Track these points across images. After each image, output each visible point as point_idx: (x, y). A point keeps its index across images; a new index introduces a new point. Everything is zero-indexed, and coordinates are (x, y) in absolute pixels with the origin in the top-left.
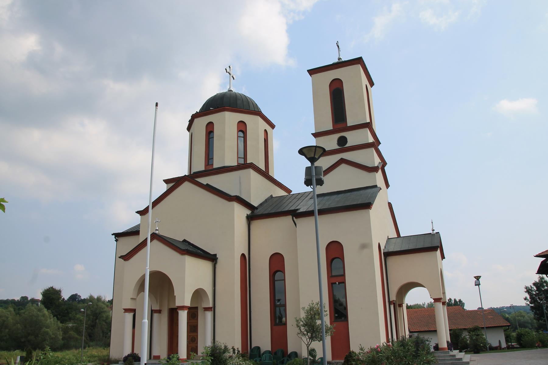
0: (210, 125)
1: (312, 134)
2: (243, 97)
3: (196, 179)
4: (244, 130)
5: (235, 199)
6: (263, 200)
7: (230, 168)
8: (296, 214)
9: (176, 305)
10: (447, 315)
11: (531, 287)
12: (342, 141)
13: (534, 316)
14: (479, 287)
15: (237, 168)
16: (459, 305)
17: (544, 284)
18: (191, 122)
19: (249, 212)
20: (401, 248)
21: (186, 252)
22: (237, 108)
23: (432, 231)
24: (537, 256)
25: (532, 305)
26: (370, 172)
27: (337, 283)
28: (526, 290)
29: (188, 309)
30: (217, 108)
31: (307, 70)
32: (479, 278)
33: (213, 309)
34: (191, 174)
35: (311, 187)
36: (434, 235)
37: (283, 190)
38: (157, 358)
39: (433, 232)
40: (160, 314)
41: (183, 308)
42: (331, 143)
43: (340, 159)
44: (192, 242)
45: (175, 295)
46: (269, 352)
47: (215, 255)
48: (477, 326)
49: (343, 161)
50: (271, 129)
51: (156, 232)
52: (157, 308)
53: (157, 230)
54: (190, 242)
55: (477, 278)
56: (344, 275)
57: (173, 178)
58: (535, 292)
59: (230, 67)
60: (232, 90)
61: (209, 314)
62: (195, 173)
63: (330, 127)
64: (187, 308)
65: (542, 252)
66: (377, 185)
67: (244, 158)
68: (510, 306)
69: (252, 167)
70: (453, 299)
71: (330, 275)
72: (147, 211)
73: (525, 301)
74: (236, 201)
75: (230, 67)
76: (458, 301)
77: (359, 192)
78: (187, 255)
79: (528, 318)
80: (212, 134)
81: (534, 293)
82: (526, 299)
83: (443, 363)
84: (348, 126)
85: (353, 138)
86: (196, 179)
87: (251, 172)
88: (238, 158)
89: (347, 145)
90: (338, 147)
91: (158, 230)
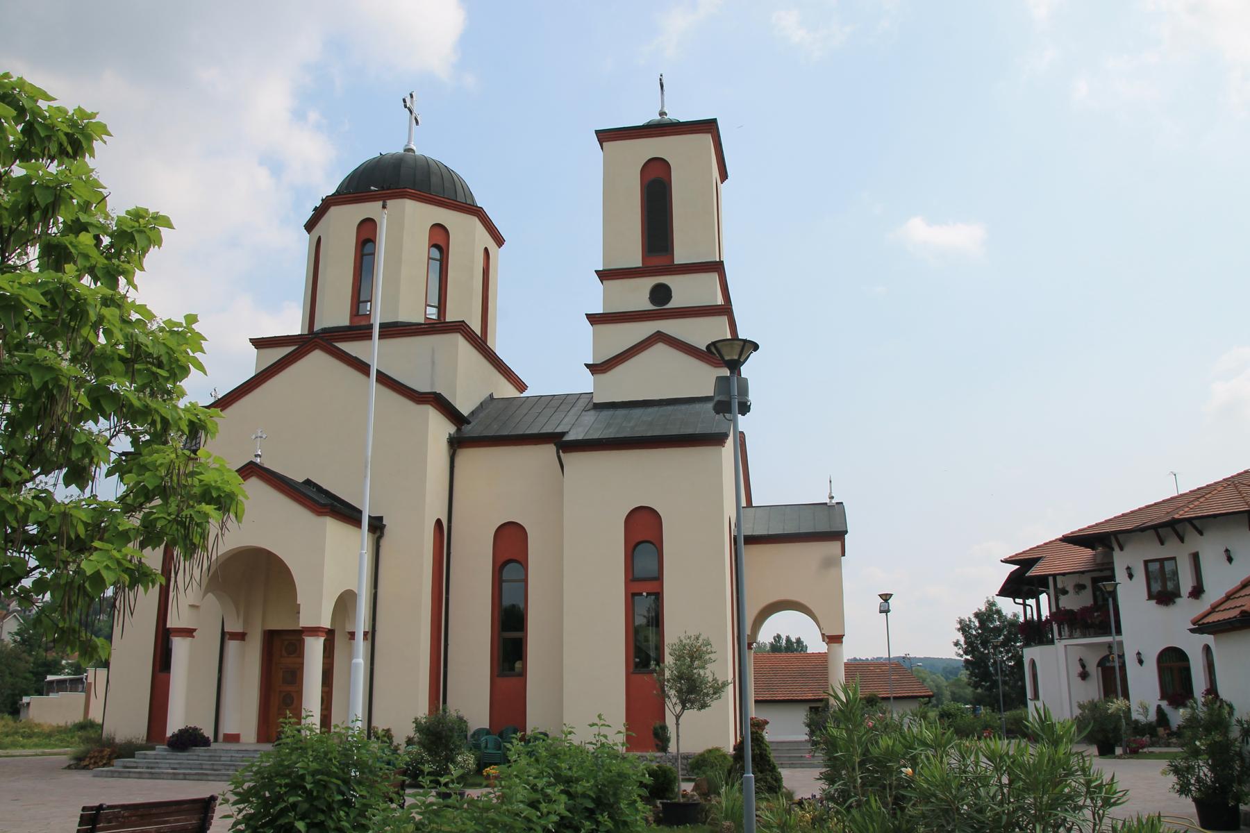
0: (366, 235)
2: (442, 170)
4: (441, 244)
5: (431, 399)
8: (564, 444)
9: (301, 625)
11: (970, 621)
12: (661, 294)
13: (970, 679)
14: (887, 615)
16: (796, 650)
17: (995, 616)
20: (768, 530)
22: (430, 194)
23: (830, 498)
24: (1006, 561)
25: (969, 657)
26: (716, 367)
27: (645, 594)
28: (959, 626)
29: (324, 634)
30: (388, 189)
31: (596, 131)
32: (888, 598)
34: (316, 329)
35: (724, 416)
37: (511, 383)
38: (234, 738)
41: (314, 631)
42: (637, 295)
43: (655, 333)
44: (325, 487)
45: (298, 603)
46: (488, 732)
48: (875, 695)
50: (496, 245)
52: (234, 626)
53: (259, 455)
54: (321, 485)
55: (884, 598)
56: (659, 578)
57: (288, 336)
58: (975, 631)
59: (411, 96)
60: (414, 148)
62: (325, 331)
63: (636, 261)
64: (322, 631)
65: (1017, 555)
68: (904, 658)
69: (463, 331)
70: (784, 637)
71: (631, 578)
73: (956, 649)
75: (411, 96)
76: (794, 640)
77: (691, 406)
78: (331, 516)
79: (931, 683)
80: (369, 245)
81: (974, 633)
82: (957, 644)
85: (685, 290)
87: (460, 340)
88: (427, 305)
89: (669, 306)
91: (260, 456)
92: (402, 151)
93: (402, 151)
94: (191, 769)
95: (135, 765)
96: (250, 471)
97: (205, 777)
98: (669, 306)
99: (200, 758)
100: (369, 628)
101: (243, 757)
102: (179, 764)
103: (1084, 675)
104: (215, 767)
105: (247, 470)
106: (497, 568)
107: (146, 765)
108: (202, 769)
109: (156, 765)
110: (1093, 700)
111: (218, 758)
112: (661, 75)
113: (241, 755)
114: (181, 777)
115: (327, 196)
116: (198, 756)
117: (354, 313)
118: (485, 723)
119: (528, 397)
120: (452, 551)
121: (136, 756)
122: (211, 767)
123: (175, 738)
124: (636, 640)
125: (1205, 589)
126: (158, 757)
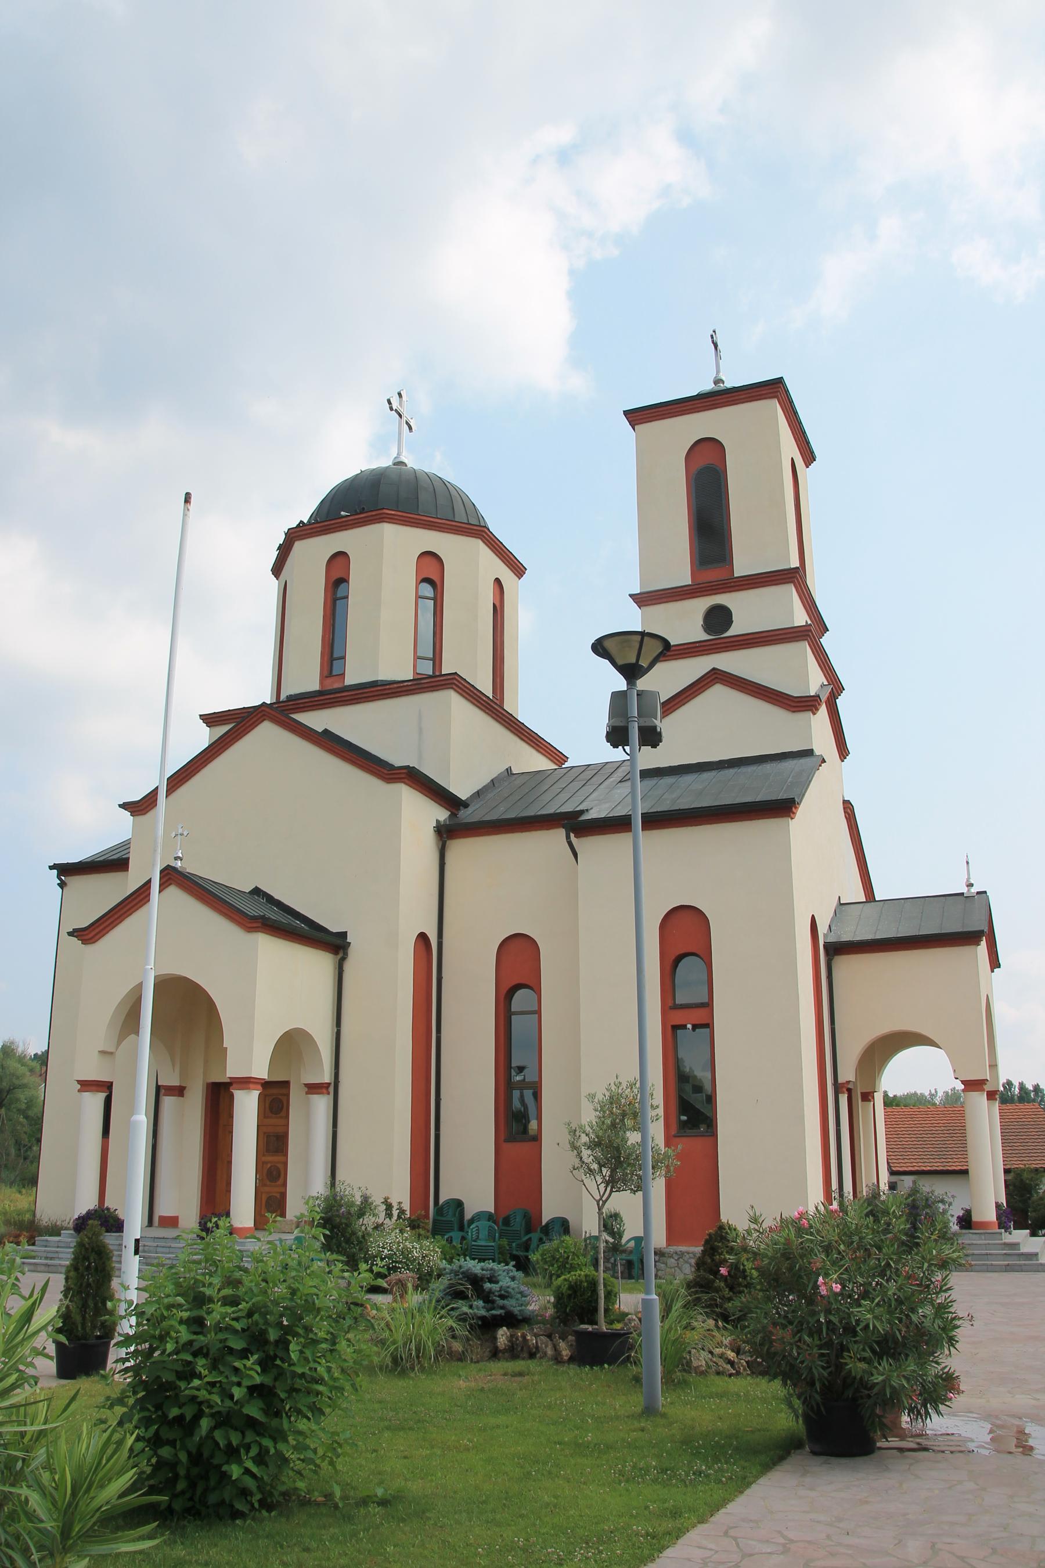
0: (340, 559)
1: (630, 596)
3: (295, 716)
4: (435, 578)
6: (486, 780)
7: (392, 686)
9: (228, 1076)
10: (999, 1128)
15: (413, 687)
16: (1034, 1101)
18: (285, 550)
19: (442, 814)
21: (259, 925)
23: (967, 886)
26: (794, 712)
27: (689, 1026)
29: (260, 1087)
35: (624, 750)
39: (968, 890)
40: (180, 1098)
41: (245, 1083)
44: (276, 897)
46: (490, 1217)
47: (344, 935)
49: (716, 678)
51: (176, 864)
52: (171, 1080)
53: (179, 857)
56: (708, 1005)
59: (400, 395)
60: (406, 461)
61: (321, 1104)
62: (291, 698)
63: (684, 578)
67: (434, 660)
74: (406, 780)
75: (400, 395)
77: (760, 767)
80: (343, 586)
83: (984, 1265)
84: (735, 575)
86: (295, 716)
87: (453, 699)
88: (416, 658)
90: (705, 637)
96: (167, 878)
100: (331, 1079)
101: (157, 1246)
103: (125, 1247)
106: (502, 997)
107: (45, 1255)
113: (155, 1244)
115: (289, 529)
117: (326, 673)
120: (444, 975)
121: (37, 1243)
123: (81, 1221)
124: (680, 1090)
125: (254, 887)
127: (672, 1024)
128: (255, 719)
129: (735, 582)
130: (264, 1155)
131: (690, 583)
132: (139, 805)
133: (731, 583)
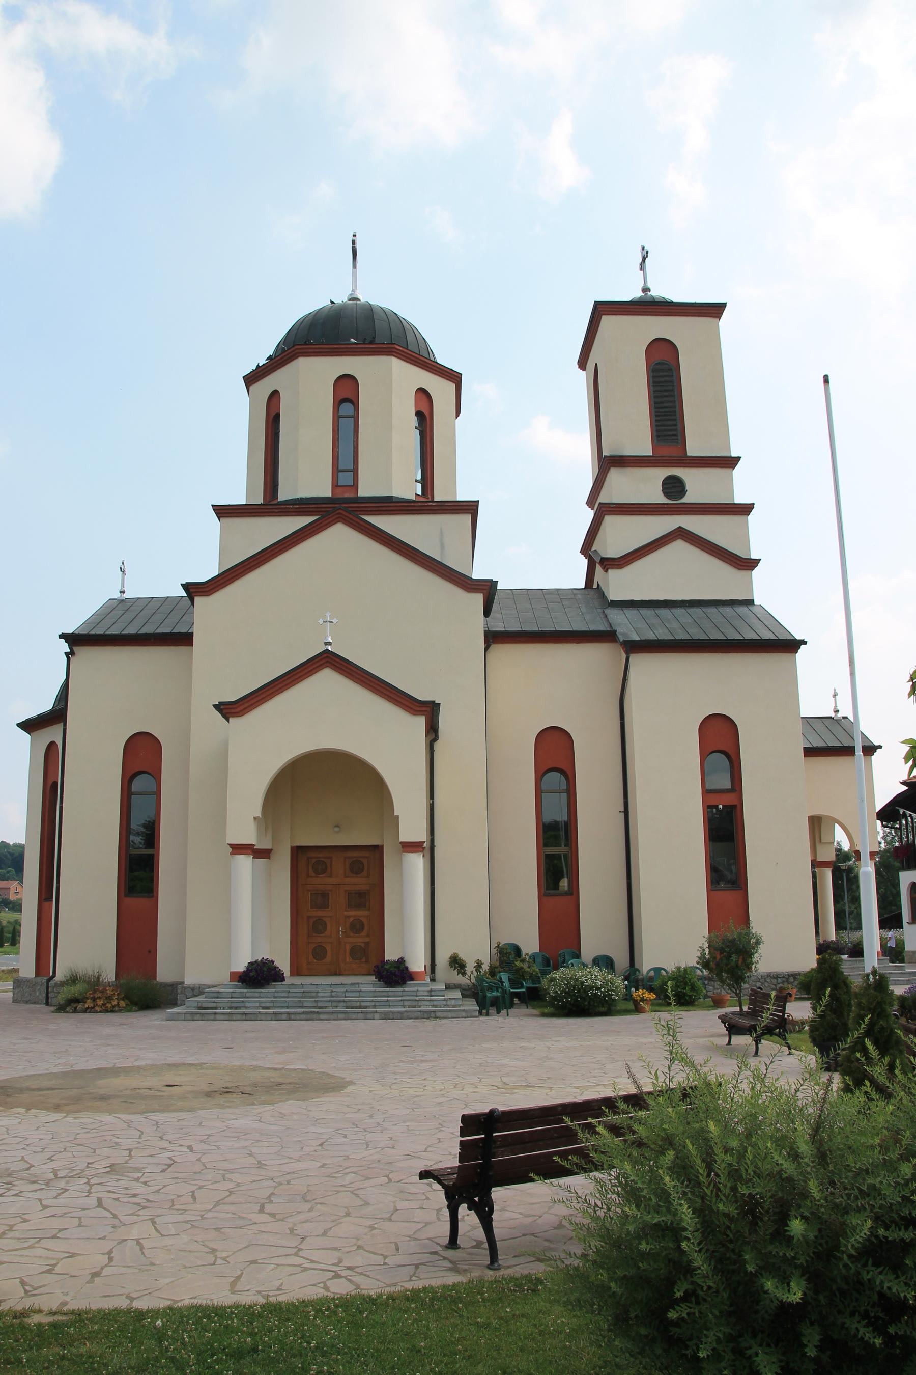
4: (426, 412)
12: (674, 487)
23: (835, 712)
26: (739, 569)
33: (428, 849)
36: (838, 721)
39: (836, 715)
45: (396, 814)
61: (417, 863)
66: (753, 601)
72: (753, 566)
89: (684, 500)
90: (664, 500)
92: (345, 300)
93: (345, 300)
94: (288, 1007)
95: (214, 1005)
97: (315, 1016)
98: (684, 500)
99: (291, 995)
101: (347, 991)
102: (271, 1002)
104: (319, 1004)
105: (321, 660)
107: (229, 1005)
108: (302, 1007)
109: (242, 1005)
110: (98, 978)
111: (314, 994)
112: (354, 236)
113: (345, 990)
114: (284, 1017)
116: (289, 992)
118: (536, 949)
119: (153, 598)
122: (315, 1004)
126: (234, 995)
127: (708, 804)
128: (330, 520)
129: (690, 460)
130: (346, 910)
131: (651, 454)
132: (205, 586)
133: (686, 460)
